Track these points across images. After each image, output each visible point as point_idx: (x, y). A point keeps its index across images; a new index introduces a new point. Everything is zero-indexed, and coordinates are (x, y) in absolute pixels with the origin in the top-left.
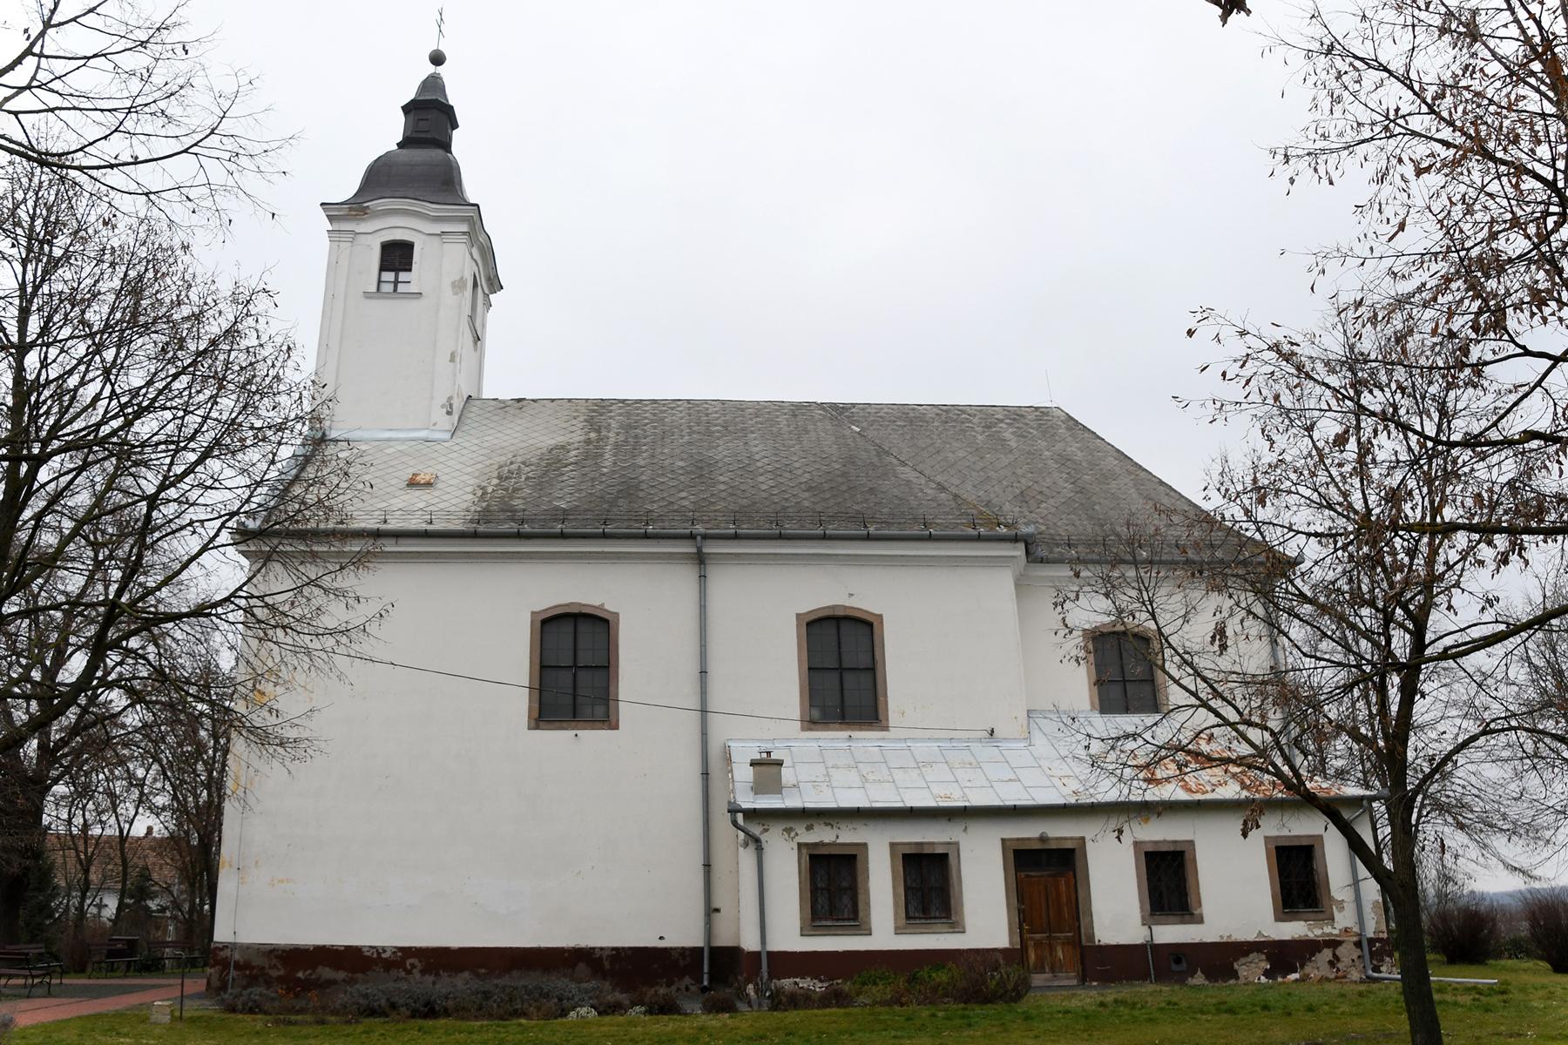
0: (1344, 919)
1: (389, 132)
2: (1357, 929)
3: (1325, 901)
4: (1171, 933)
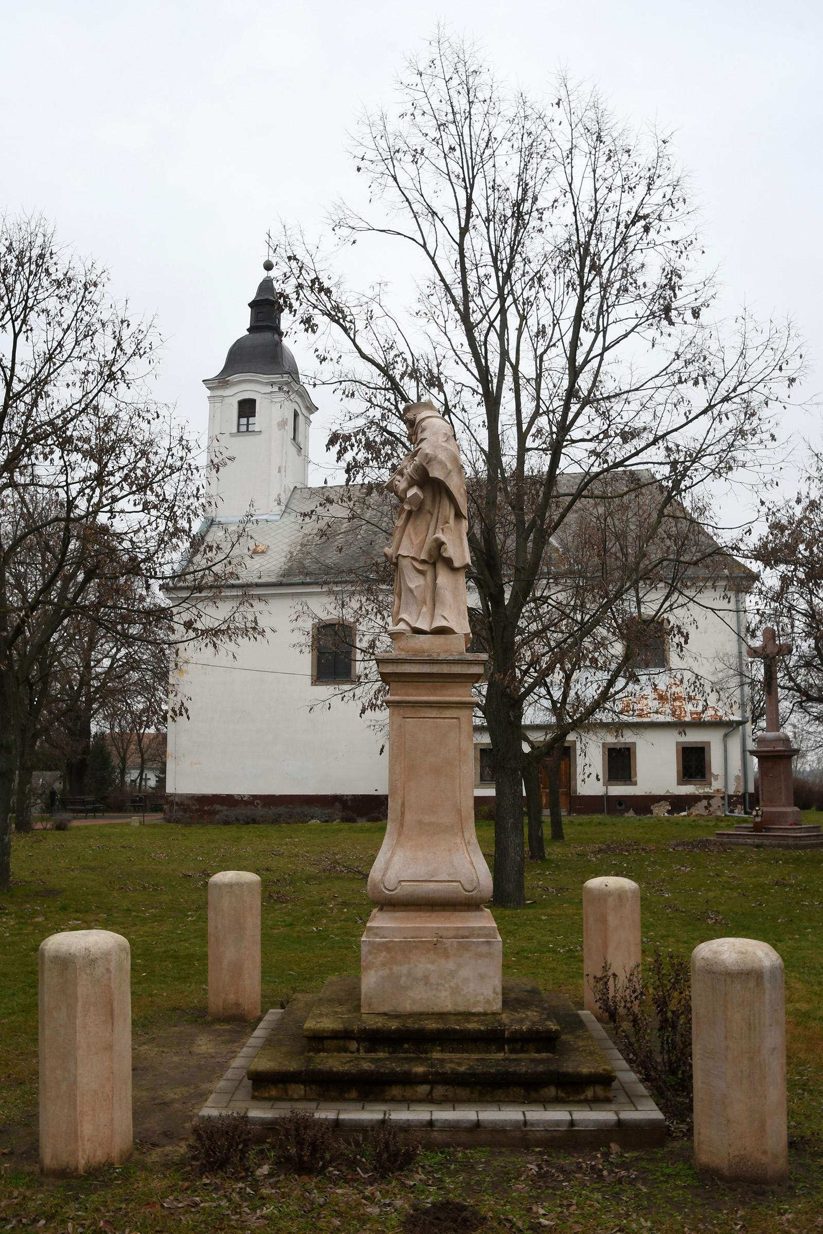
0: (717, 785)
1: (239, 324)
2: (723, 790)
3: (707, 776)
4: (618, 790)
